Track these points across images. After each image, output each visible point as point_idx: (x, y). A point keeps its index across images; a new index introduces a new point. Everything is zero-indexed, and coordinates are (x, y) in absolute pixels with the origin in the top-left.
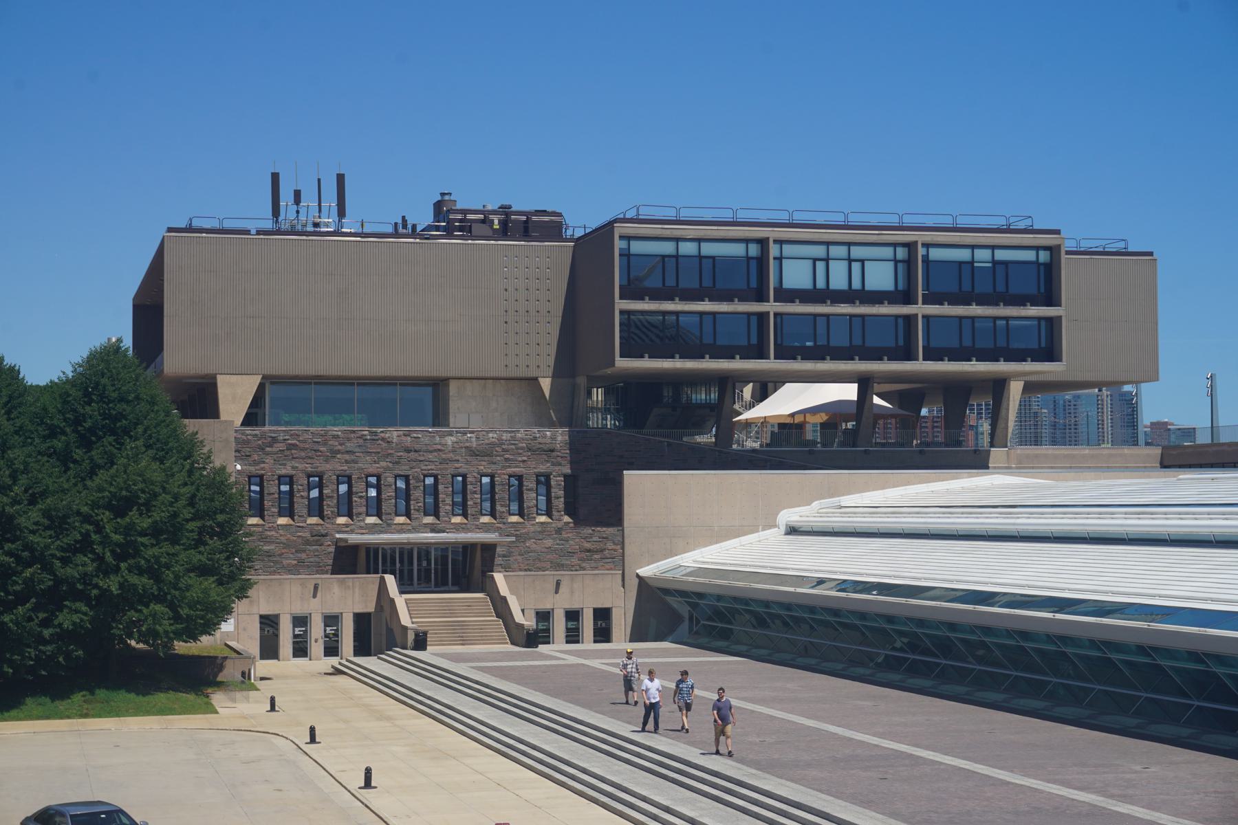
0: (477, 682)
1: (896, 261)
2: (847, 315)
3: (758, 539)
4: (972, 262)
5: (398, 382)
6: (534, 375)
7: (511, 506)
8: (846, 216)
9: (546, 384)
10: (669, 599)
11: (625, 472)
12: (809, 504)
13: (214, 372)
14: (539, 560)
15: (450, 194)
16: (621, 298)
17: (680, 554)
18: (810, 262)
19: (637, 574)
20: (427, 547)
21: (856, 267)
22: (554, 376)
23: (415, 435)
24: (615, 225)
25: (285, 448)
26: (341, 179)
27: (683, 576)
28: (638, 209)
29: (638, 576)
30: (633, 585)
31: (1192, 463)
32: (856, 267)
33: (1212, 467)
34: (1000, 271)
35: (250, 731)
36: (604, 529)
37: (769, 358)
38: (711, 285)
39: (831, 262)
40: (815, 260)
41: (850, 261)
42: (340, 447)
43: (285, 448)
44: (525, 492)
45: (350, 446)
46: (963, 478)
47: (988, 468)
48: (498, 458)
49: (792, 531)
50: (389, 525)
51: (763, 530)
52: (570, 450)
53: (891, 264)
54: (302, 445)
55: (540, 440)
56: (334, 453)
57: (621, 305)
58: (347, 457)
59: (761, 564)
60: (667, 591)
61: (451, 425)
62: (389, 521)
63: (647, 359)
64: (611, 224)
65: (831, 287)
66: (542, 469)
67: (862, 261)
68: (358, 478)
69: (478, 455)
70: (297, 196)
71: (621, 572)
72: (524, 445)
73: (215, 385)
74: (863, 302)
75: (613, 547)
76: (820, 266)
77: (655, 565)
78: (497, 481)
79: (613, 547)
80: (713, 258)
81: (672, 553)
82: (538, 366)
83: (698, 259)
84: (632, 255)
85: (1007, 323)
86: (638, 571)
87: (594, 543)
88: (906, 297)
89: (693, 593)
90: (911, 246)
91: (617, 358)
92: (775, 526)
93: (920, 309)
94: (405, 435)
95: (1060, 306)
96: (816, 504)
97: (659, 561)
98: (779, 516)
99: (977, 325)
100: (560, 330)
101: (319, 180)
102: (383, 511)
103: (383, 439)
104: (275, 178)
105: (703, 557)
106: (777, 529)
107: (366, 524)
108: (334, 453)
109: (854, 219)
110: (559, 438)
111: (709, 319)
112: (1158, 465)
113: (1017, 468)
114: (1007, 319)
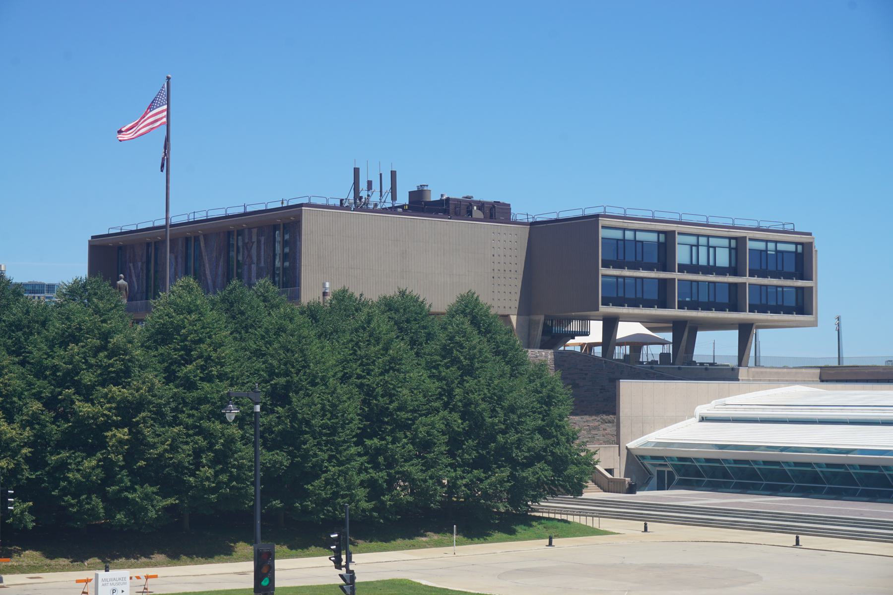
0: (875, 521)
1: (730, 248)
2: (706, 282)
3: (685, 425)
4: (766, 251)
6: (506, 313)
8: (759, 223)
9: (514, 319)
10: (646, 462)
11: (621, 380)
15: (427, 186)
16: (602, 267)
17: (647, 434)
18: (688, 247)
19: (627, 447)
21: (711, 250)
22: (518, 315)
24: (600, 218)
26: (393, 174)
27: (640, 446)
28: (605, 208)
29: (627, 448)
30: (624, 453)
31: (848, 379)
32: (711, 250)
33: (857, 382)
34: (779, 255)
35: (826, 550)
36: (574, 417)
38: (781, 269)
39: (700, 247)
40: (692, 246)
41: (709, 247)
46: (781, 387)
47: (738, 380)
49: (703, 419)
51: (688, 419)
52: (555, 364)
53: (727, 250)
55: (539, 358)
57: (603, 271)
59: (886, 445)
60: (643, 457)
63: (611, 306)
64: (597, 216)
65: (717, 265)
67: (715, 248)
70: (370, 184)
71: (618, 446)
76: (694, 249)
77: (635, 441)
80: (642, 242)
81: (643, 434)
82: (510, 308)
83: (634, 242)
85: (783, 290)
86: (627, 445)
88: (734, 270)
90: (741, 241)
91: (600, 306)
92: (693, 416)
93: (747, 280)
95: (812, 280)
96: (713, 402)
97: (637, 438)
98: (696, 410)
99: (769, 290)
100: (522, 282)
101: (381, 175)
104: (356, 171)
106: (694, 418)
109: (712, 221)
110: (549, 357)
111: (694, 284)
112: (818, 379)
113: (754, 380)
114: (782, 287)
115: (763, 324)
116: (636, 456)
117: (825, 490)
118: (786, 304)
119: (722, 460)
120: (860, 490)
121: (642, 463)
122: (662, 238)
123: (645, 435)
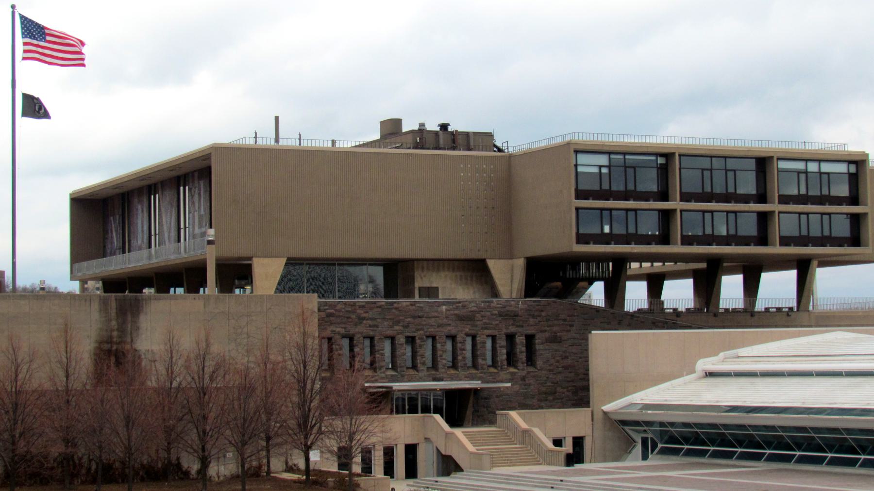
5: (368, 263)
7: (290, 355)
12: (717, 355)
13: (251, 256)
14: (511, 401)
19: (602, 410)
20: (402, 394)
21: (731, 175)
23: (418, 305)
25: (325, 316)
32: (731, 175)
37: (678, 245)
42: (364, 315)
43: (325, 316)
44: (498, 348)
45: (370, 314)
48: (479, 322)
49: (711, 374)
50: (403, 376)
54: (337, 314)
56: (361, 319)
58: (370, 322)
61: (440, 298)
62: (402, 373)
66: (512, 329)
68: (380, 339)
69: (463, 320)
72: (496, 312)
73: (250, 267)
74: (737, 202)
75: (561, 390)
78: (479, 340)
79: (561, 390)
80: (828, 174)
84: (612, 166)
87: (548, 388)
89: (750, 426)
92: (693, 372)
94: (412, 305)
96: (722, 355)
102: (398, 365)
103: (396, 309)
105: (647, 396)
107: (386, 375)
108: (361, 319)
115: (828, 259)
116: (615, 420)
117: (709, 453)
118: (740, 233)
119: (810, 428)
120: (738, 453)
121: (622, 428)
122: (853, 169)
123: (628, 395)
